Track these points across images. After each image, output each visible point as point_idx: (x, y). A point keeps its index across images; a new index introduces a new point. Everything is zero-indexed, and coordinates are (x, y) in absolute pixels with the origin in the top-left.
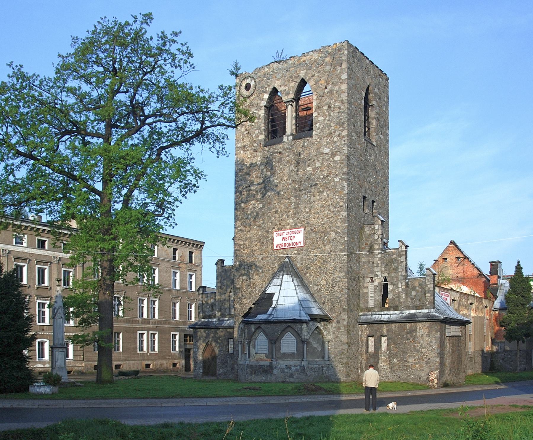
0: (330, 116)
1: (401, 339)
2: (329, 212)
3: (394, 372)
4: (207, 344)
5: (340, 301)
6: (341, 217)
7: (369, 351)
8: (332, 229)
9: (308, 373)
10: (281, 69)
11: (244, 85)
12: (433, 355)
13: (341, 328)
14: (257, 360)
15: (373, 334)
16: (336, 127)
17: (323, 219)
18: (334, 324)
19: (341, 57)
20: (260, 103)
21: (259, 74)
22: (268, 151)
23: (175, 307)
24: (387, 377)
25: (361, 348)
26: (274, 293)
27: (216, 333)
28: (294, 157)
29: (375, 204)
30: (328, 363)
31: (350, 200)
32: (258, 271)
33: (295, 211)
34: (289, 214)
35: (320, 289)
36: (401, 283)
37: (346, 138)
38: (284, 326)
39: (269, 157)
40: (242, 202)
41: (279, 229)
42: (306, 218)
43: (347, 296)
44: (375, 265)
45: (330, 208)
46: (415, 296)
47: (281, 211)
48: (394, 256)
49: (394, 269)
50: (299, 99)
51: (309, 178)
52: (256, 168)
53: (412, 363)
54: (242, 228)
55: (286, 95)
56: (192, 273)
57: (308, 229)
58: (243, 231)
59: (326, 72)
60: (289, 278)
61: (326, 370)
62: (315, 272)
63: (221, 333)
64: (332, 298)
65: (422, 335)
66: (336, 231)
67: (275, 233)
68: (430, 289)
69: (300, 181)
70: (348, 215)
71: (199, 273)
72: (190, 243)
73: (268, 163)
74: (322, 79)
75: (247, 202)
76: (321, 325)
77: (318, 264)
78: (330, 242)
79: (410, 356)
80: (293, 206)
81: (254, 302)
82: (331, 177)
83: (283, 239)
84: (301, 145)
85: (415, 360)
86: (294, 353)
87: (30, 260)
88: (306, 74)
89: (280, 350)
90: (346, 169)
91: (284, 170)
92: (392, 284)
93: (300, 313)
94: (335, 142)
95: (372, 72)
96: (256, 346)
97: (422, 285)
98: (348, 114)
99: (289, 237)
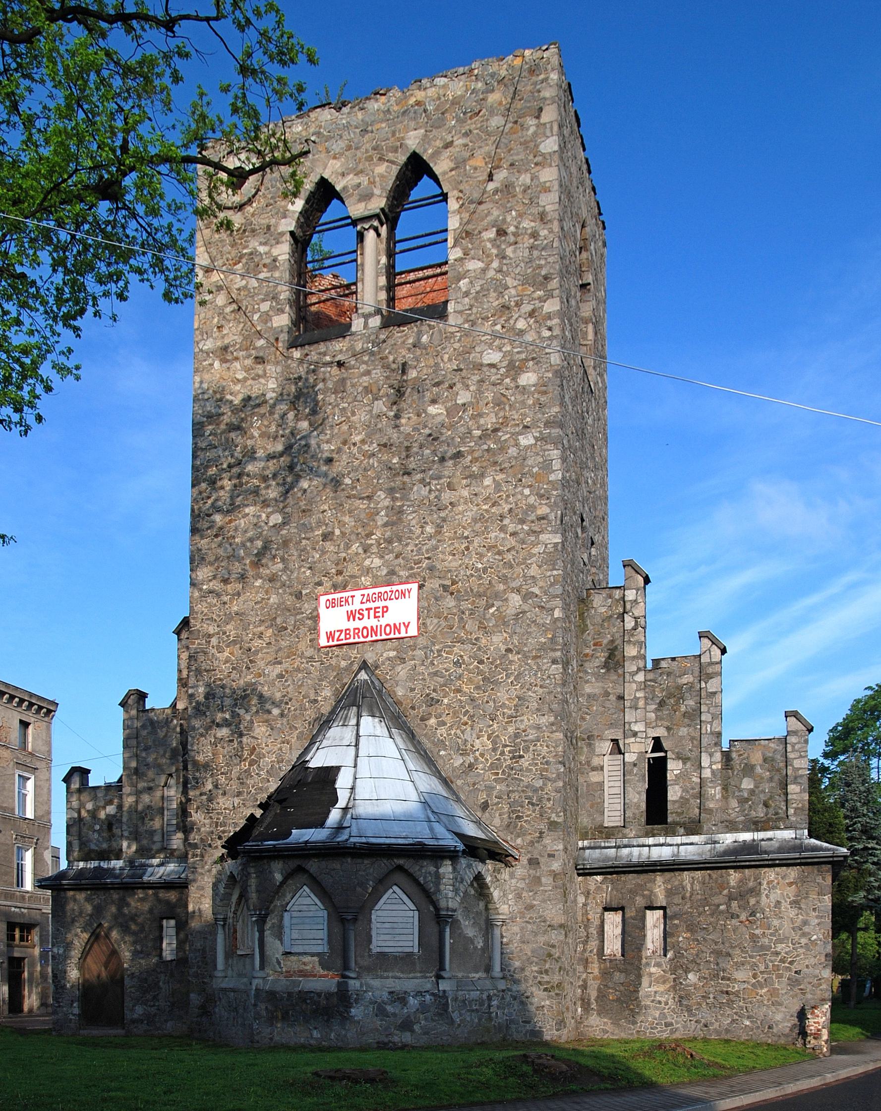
0: (504, 258)
1: (712, 915)
2: (502, 535)
3: (689, 1010)
4: (92, 934)
5: (540, 800)
6: (540, 549)
7: (607, 951)
8: (514, 584)
9: (455, 1016)
10: (347, 127)
12: (813, 961)
13: (543, 880)
14: (289, 974)
15: (624, 903)
16: (523, 290)
17: (481, 556)
18: (521, 869)
19: (539, 91)
20: (276, 226)
22: (301, 361)
24: (667, 1025)
25: (585, 942)
26: (338, 768)
27: (123, 903)
28: (387, 378)
30: (502, 985)
32: (269, 712)
33: (389, 533)
34: (369, 542)
35: (471, 766)
36: (711, 755)
38: (384, 865)
39: (307, 379)
40: (219, 510)
42: (427, 551)
43: (561, 784)
44: (627, 704)
45: (506, 522)
46: (752, 792)
47: (343, 534)
48: (686, 679)
49: (685, 715)
51: (435, 435)
52: (262, 410)
53: (746, 986)
54: (216, 585)
55: (360, 201)
56: (26, 774)
57: (433, 584)
58: (218, 595)
59: (489, 134)
60: (377, 725)
61: (498, 1007)
62: (454, 713)
63: (138, 903)
64: (513, 791)
65: (778, 902)
66: (524, 591)
67: (323, 599)
68: (800, 772)
69: (406, 444)
71: (42, 775)
72: (22, 701)
74: (479, 154)
75: (233, 509)
76: (487, 868)
77: (465, 688)
78: (505, 624)
79: (739, 965)
80: (382, 518)
81: (263, 797)
82: (507, 433)
83: (351, 616)
84: (411, 341)
85: (755, 976)
86: (410, 955)
88: (425, 139)
89: (370, 942)
90: (556, 409)
91: (353, 413)
92: (679, 757)
93: (431, 829)
94: (521, 333)
96: (287, 930)
97: (773, 760)
99: (368, 609)
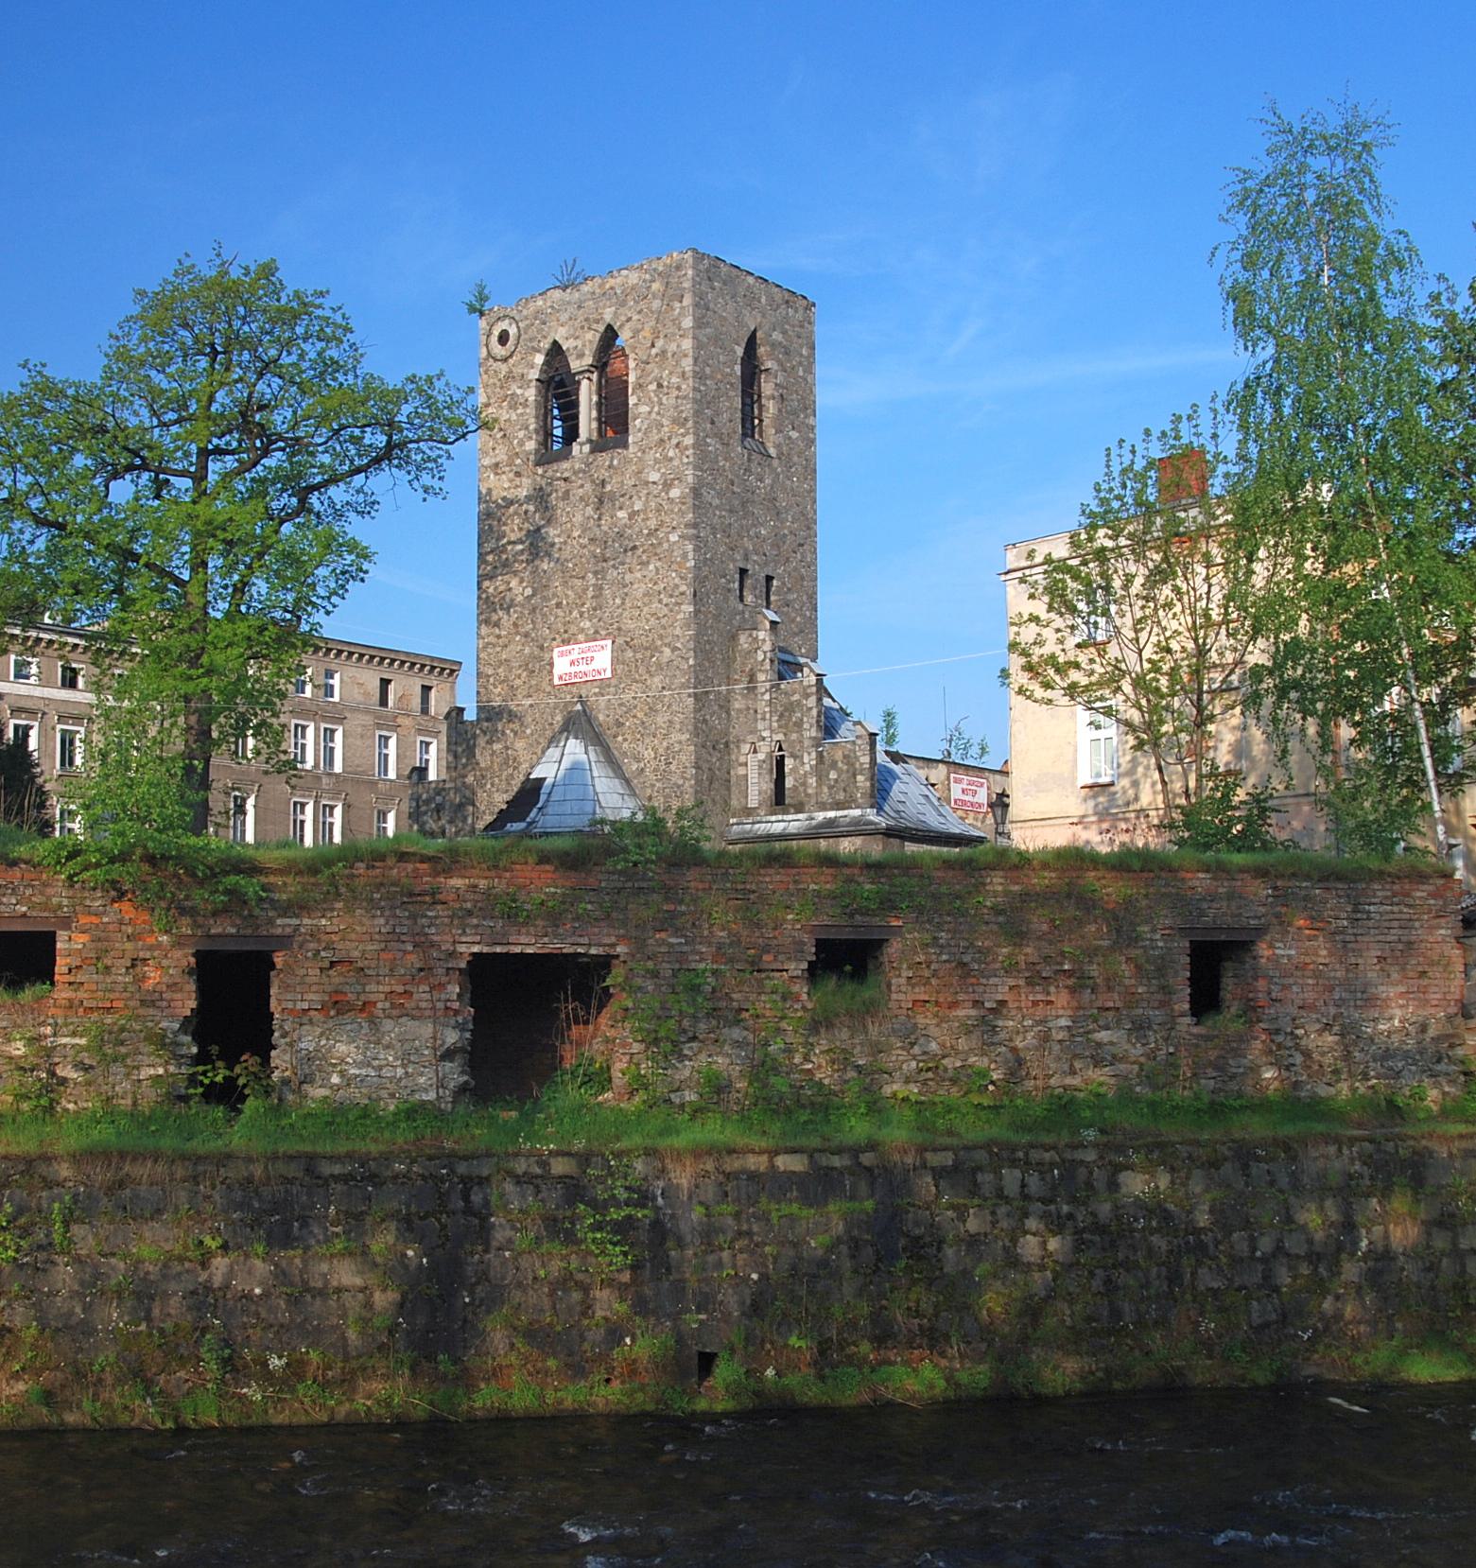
6: (680, 616)
11: (496, 333)
17: (648, 620)
21: (525, 312)
22: (542, 476)
23: (385, 822)
29: (775, 582)
31: (699, 580)
37: (691, 451)
41: (566, 642)
46: (836, 781)
48: (796, 697)
49: (795, 724)
50: (605, 364)
67: (556, 650)
70: (697, 612)
73: (540, 497)
80: (590, 593)
83: (572, 663)
87: (44, 714)
92: (794, 756)
94: (671, 459)
95: (763, 300)
98: (695, 401)
